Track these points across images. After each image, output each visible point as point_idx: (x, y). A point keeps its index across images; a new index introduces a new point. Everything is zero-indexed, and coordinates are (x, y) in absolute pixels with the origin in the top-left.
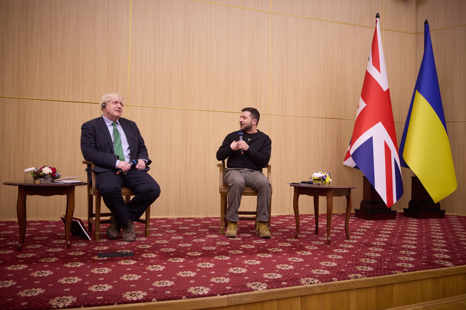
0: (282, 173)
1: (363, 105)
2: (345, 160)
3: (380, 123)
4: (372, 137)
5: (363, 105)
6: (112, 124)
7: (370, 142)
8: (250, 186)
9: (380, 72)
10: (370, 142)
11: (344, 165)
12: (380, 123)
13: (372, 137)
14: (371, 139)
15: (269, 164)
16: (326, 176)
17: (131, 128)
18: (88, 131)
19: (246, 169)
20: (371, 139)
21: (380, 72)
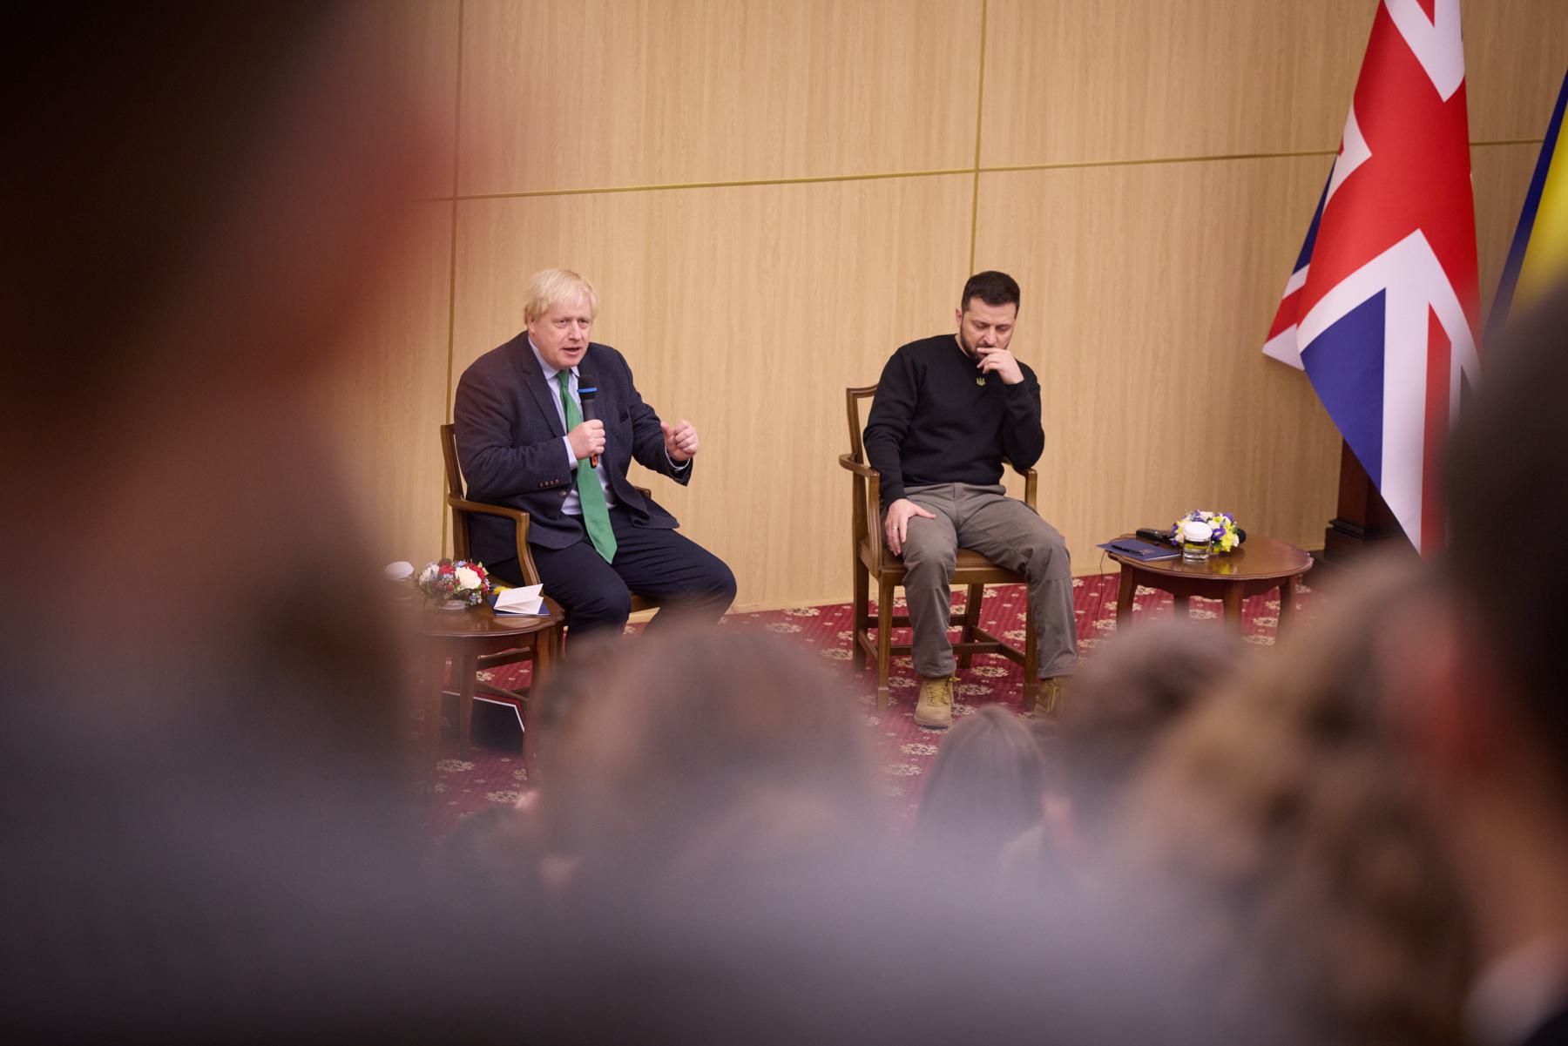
0: (1075, 500)
1: (1358, 152)
2: (1273, 334)
3: (1418, 234)
4: (1383, 293)
5: (1358, 152)
6: (556, 377)
7: (1373, 311)
8: (981, 554)
9: (1431, 17)
10: (1373, 311)
11: (1271, 361)
12: (1418, 234)
13: (1383, 293)
14: (1380, 298)
15: (1036, 467)
16: (1222, 529)
17: (605, 373)
18: (494, 405)
19: (960, 486)
20: (1380, 298)
21: (1431, 17)
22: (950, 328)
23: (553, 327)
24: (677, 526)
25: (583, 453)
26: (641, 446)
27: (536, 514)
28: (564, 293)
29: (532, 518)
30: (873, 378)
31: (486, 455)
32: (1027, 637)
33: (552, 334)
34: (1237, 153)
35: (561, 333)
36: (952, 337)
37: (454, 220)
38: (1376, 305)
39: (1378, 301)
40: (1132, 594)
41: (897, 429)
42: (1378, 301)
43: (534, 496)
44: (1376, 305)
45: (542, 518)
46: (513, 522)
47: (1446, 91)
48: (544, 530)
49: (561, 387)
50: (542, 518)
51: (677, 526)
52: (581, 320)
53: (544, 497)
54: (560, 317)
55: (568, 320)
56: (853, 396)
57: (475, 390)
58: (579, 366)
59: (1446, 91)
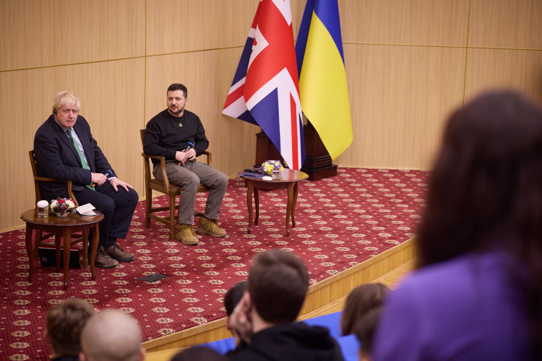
2: (225, 107)
4: (276, 89)
7: (274, 95)
10: (274, 95)
13: (276, 89)
14: (276, 91)
20: (276, 91)
23: (63, 113)
26: (98, 160)
28: (69, 101)
32: (26, 244)
33: (63, 116)
34: (106, 62)
35: (66, 115)
37: (469, 18)
38: (275, 93)
39: (275, 92)
42: (275, 92)
44: (275, 93)
47: (289, 24)
52: (73, 111)
54: (65, 109)
55: (69, 110)
58: (73, 127)
59: (289, 24)
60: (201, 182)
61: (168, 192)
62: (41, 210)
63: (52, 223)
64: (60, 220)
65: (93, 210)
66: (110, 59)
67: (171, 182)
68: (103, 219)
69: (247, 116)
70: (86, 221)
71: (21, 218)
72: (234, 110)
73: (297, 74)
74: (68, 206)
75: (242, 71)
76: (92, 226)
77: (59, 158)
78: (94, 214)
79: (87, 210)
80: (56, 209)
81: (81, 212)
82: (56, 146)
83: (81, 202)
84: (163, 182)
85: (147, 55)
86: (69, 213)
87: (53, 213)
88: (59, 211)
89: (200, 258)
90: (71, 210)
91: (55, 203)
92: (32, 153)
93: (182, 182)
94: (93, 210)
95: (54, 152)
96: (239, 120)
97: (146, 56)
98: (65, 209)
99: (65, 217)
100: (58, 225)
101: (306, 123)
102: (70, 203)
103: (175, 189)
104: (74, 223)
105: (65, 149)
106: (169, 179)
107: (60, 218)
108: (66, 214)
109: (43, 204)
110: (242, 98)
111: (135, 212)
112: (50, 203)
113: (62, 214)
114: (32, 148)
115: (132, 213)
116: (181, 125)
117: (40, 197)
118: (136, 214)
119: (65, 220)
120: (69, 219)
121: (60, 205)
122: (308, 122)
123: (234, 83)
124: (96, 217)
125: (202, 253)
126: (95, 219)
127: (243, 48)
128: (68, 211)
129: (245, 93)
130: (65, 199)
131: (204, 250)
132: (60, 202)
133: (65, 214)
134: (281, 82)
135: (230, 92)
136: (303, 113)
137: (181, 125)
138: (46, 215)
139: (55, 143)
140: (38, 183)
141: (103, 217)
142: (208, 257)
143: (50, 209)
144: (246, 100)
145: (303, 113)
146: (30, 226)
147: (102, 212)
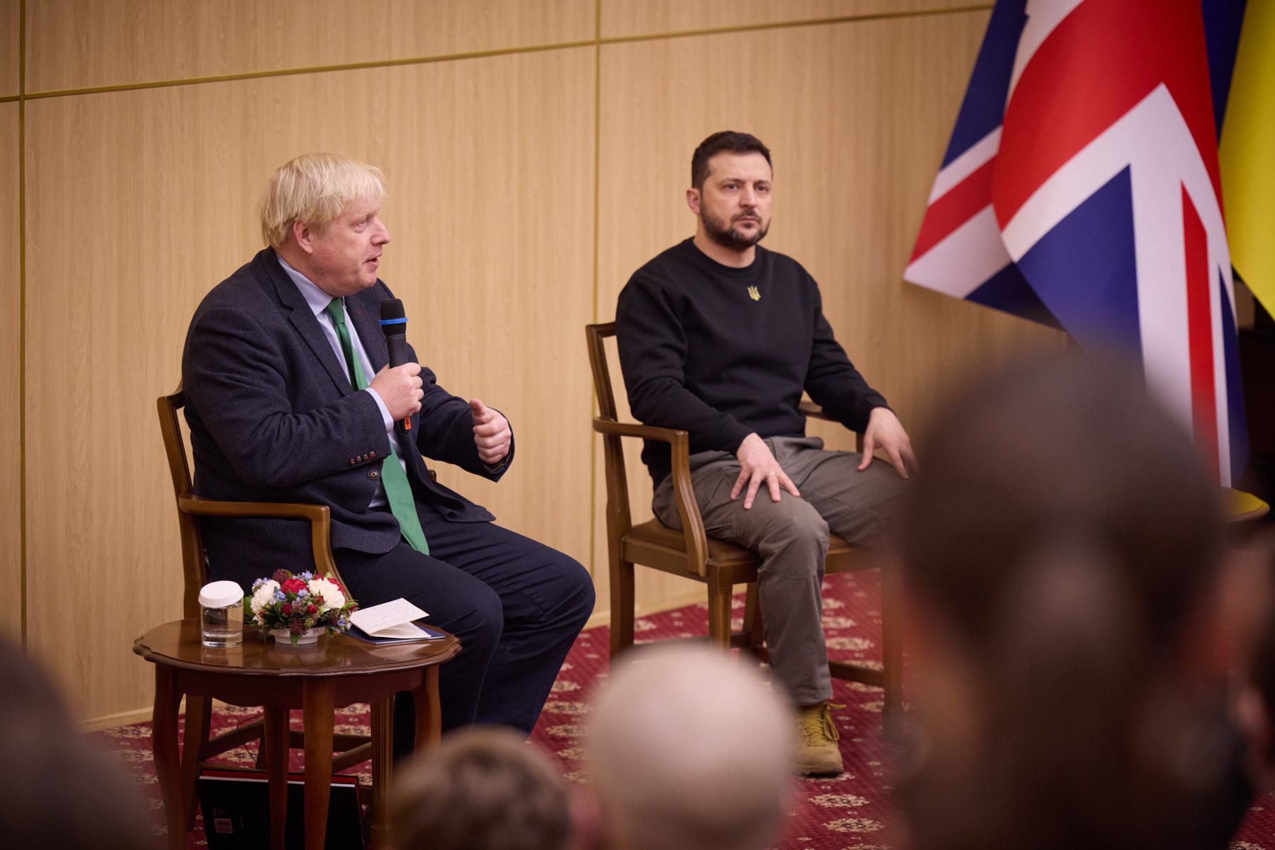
2: (918, 252)
7: (1116, 196)
10: (1116, 196)
18: (265, 355)
22: (686, 227)
24: (494, 519)
25: (401, 412)
27: (337, 507)
29: (334, 515)
30: (608, 315)
31: (274, 424)
33: (352, 243)
36: (688, 244)
40: (886, 700)
41: (492, 435)
43: (337, 481)
45: (344, 512)
46: (307, 524)
48: (352, 529)
49: (335, 324)
50: (344, 512)
51: (494, 519)
53: (337, 481)
56: (597, 333)
57: (219, 339)
60: (833, 532)
61: (702, 572)
62: (217, 618)
63: (258, 668)
64: (288, 657)
65: (419, 623)
66: (459, 51)
67: (712, 535)
68: (458, 657)
69: (1009, 289)
70: (390, 662)
71: (137, 652)
72: (953, 266)
73: (1209, 121)
74: (319, 600)
75: (981, 110)
76: (415, 683)
77: (278, 415)
78: (423, 634)
79: (395, 620)
80: (273, 616)
81: (370, 630)
82: (280, 360)
83: (365, 596)
84: (681, 531)
85: (605, 34)
86: (322, 630)
87: (258, 634)
88: (286, 624)
89: (835, 825)
90: (330, 620)
91: (267, 592)
92: (168, 405)
93: (759, 540)
94: (419, 623)
95: (271, 381)
96: (975, 308)
97: (599, 42)
98: (311, 612)
99: (307, 649)
100: (284, 673)
101: (1249, 321)
102: (328, 592)
103: (727, 560)
104: (346, 667)
105: (312, 376)
106: (705, 516)
107: (289, 649)
108: (311, 636)
109: (221, 593)
110: (988, 214)
111: (565, 667)
112: (248, 592)
113: (296, 634)
114: (172, 383)
115: (553, 675)
116: (755, 295)
117: (202, 568)
118: (570, 676)
119: (309, 658)
120: (322, 656)
121: (290, 599)
122: (1260, 310)
123: (951, 156)
124: (434, 647)
125: (844, 810)
126: (422, 654)
127: (985, 18)
128: (319, 623)
129: (999, 191)
130: (308, 575)
131: (852, 798)
132: (289, 589)
133: (310, 633)
134: (1146, 144)
135: (937, 193)
136: (1236, 277)
137: (755, 295)
138: (232, 637)
139: (276, 348)
140: (192, 523)
141: (458, 647)
142: (867, 822)
143: (248, 615)
144: (1004, 219)
145: (1236, 277)
146: (172, 680)
147: (449, 629)
